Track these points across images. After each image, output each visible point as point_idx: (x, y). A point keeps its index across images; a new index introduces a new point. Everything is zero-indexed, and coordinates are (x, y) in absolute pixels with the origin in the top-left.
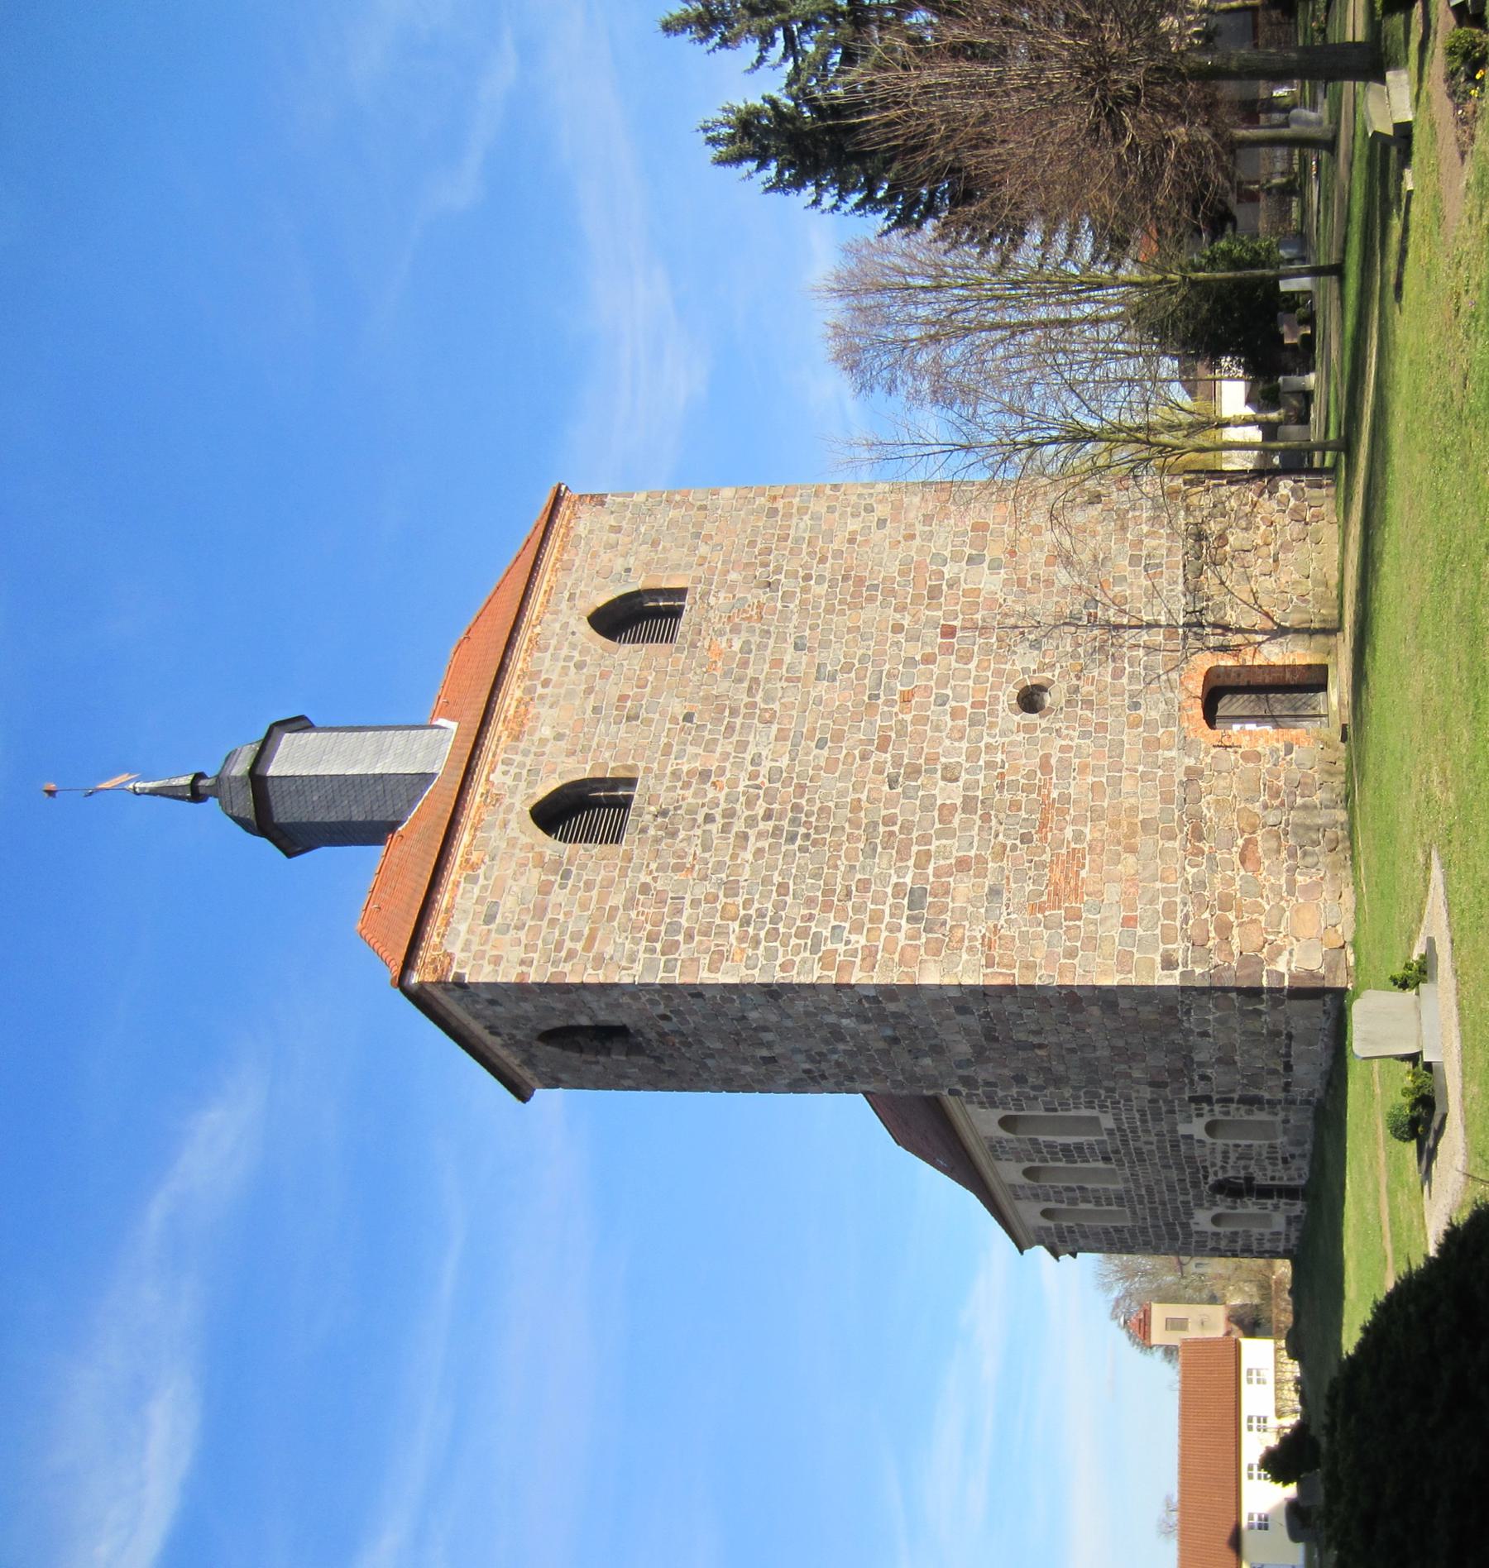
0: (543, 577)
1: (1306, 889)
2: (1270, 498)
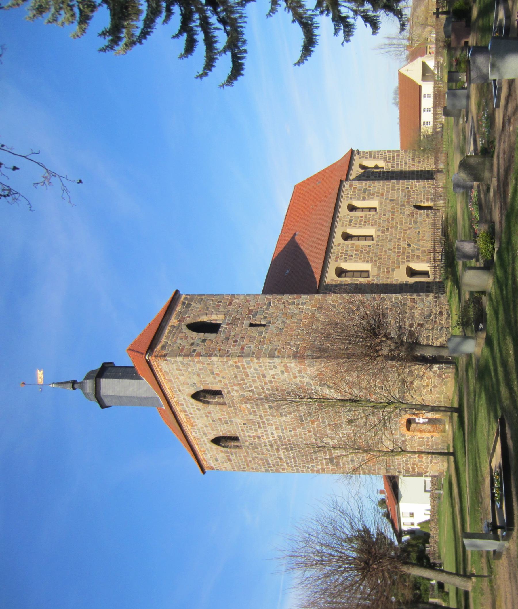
0: (164, 385)
1: (435, 463)
2: (430, 371)
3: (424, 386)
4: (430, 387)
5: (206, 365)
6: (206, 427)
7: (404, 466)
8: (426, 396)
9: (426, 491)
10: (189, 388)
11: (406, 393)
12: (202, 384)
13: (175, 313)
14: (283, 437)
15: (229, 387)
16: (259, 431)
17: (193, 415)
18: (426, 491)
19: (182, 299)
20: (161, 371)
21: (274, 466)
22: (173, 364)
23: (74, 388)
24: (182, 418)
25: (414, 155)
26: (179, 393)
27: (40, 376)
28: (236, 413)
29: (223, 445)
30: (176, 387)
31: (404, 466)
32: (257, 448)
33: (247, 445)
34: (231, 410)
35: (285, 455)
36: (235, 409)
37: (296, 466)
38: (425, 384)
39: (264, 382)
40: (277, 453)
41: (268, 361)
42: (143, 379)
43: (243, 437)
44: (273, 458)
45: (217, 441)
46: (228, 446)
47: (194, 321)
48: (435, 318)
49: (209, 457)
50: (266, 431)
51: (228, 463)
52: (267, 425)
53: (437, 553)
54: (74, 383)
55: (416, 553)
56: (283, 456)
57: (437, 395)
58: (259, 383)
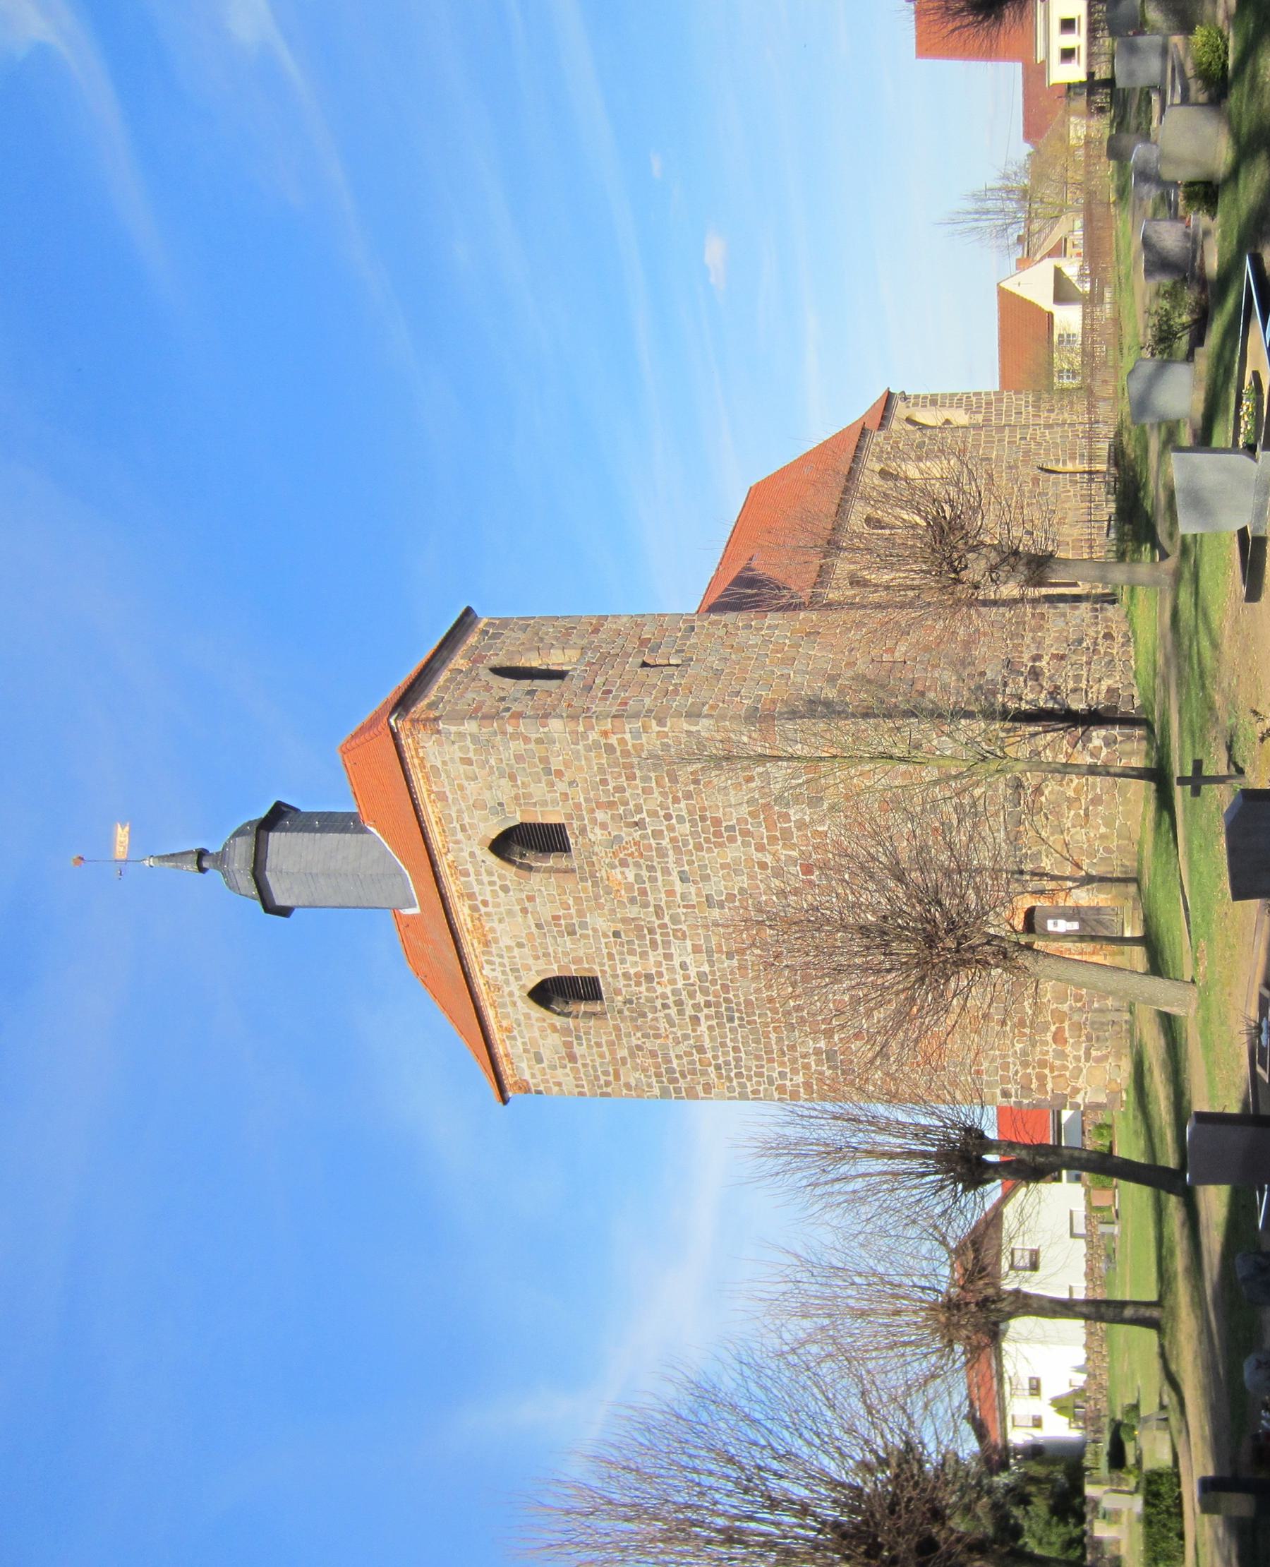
0: (426, 812)
3: (1068, 799)
4: (1083, 801)
5: (532, 746)
6: (520, 945)
7: (1016, 1073)
8: (1073, 830)
9: (1073, 1235)
10: (486, 820)
11: (1024, 823)
12: (520, 805)
13: (464, 648)
14: (710, 977)
15: (584, 813)
16: (652, 957)
17: (490, 909)
18: (1073, 1235)
19: (481, 626)
20: (423, 766)
21: (684, 1076)
22: (453, 743)
23: (202, 870)
24: (462, 917)
25: (1038, 399)
26: (460, 836)
27: (122, 839)
28: (597, 897)
29: (558, 1010)
30: (454, 815)
31: (1016, 1073)
32: (644, 1015)
33: (620, 1005)
34: (585, 890)
35: (712, 1039)
36: (595, 884)
37: (739, 1075)
38: (1071, 793)
39: (670, 796)
40: (694, 1030)
41: (686, 726)
42: (371, 833)
43: (610, 980)
44: (683, 1047)
45: (546, 993)
46: (570, 1013)
47: (508, 664)
48: (1095, 644)
49: (521, 1048)
50: (668, 957)
51: (568, 1070)
52: (672, 938)
53: (1105, 1416)
54: (202, 854)
55: (1045, 1499)
56: (707, 1044)
57: (1103, 830)
58: (660, 799)
